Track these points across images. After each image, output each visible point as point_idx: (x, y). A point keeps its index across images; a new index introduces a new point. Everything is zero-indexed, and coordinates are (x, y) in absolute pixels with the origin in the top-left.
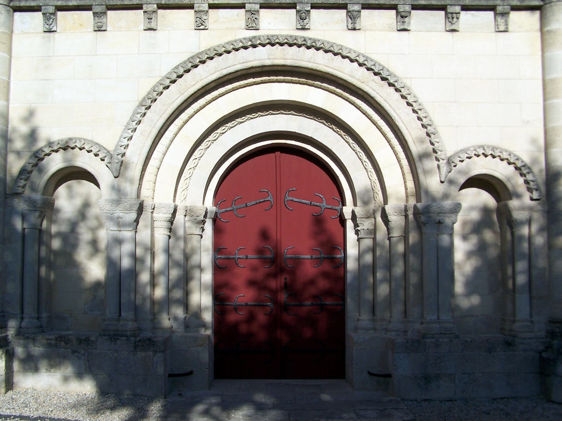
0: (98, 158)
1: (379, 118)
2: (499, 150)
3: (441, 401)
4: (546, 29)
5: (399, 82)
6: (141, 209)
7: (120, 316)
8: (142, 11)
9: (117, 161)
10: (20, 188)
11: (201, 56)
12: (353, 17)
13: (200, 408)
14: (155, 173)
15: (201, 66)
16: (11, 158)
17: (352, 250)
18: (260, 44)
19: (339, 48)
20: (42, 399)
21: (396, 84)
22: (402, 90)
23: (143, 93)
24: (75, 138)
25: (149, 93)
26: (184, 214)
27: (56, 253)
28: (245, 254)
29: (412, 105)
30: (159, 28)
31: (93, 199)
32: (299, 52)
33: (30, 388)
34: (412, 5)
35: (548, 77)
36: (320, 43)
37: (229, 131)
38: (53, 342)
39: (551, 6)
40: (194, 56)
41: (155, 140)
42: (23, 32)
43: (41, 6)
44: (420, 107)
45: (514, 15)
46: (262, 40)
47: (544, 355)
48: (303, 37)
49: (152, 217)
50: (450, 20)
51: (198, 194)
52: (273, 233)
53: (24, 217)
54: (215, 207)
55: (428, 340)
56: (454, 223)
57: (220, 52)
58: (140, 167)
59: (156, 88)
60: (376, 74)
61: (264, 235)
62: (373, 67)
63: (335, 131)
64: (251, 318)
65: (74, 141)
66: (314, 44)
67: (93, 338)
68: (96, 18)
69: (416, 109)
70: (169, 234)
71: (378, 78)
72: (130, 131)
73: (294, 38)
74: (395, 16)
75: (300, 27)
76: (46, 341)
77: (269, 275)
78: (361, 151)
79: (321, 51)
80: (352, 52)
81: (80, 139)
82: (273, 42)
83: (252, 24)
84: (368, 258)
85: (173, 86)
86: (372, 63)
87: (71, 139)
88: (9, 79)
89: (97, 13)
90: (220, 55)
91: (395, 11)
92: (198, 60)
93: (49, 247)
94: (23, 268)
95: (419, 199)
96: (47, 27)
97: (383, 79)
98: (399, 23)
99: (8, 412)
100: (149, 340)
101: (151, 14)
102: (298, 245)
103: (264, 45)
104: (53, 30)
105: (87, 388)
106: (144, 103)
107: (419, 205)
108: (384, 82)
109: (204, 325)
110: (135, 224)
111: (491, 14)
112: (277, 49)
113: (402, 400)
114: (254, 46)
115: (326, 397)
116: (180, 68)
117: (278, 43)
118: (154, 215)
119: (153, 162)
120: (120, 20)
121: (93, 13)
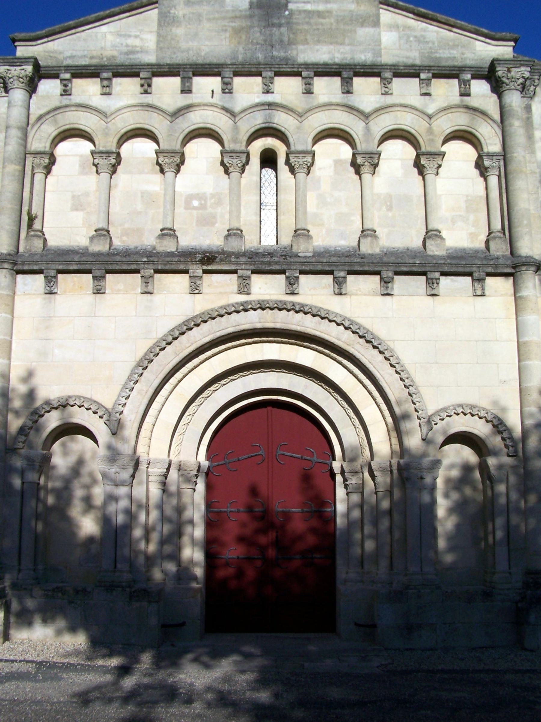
0: (97, 416)
1: (365, 378)
2: (477, 409)
3: (423, 651)
4: (518, 295)
5: (383, 345)
6: (137, 464)
7: (115, 567)
8: (139, 275)
9: (115, 419)
10: (21, 444)
11: (195, 320)
12: (339, 283)
13: (190, 656)
14: (151, 429)
15: (195, 329)
16: (10, 417)
17: (341, 507)
18: (251, 308)
19: (326, 312)
20: (39, 648)
21: (380, 346)
22: (386, 352)
23: (141, 353)
24: (75, 396)
25: (146, 354)
26: (178, 468)
27: (49, 509)
28: (234, 508)
29: (395, 367)
30: (155, 291)
31: (88, 456)
32: (288, 315)
33: (26, 639)
34: (394, 271)
35: (520, 340)
36: (308, 308)
37: (222, 388)
38: (50, 593)
39: (521, 274)
40: (189, 320)
41: (151, 398)
42: (25, 294)
43: (43, 270)
44: (402, 369)
45: (490, 281)
46: (253, 305)
47: (520, 605)
48: (292, 302)
49: (147, 472)
50: (431, 285)
51: (193, 451)
52: (263, 490)
53: (22, 473)
54: (208, 462)
55: (410, 591)
56: (435, 479)
57: (214, 316)
58: (137, 425)
59: (153, 350)
60: (361, 337)
61: (254, 492)
62: (358, 331)
63: (324, 389)
64: (240, 574)
65: (74, 399)
66: (302, 309)
67: (89, 589)
68: (96, 281)
69: (398, 370)
70: (163, 488)
71: (362, 341)
72: (127, 390)
73: (283, 303)
74: (379, 281)
75: (290, 292)
76: (43, 592)
77: (258, 531)
78: (348, 408)
79: (309, 316)
80: (338, 316)
81: (80, 397)
82: (263, 307)
83: (244, 288)
84: (356, 514)
85: (169, 348)
86: (357, 327)
87: (70, 397)
88: (11, 338)
89: (96, 277)
90: (214, 318)
91: (379, 276)
92: (193, 323)
93: (45, 503)
94: (21, 520)
95: (402, 457)
96: (48, 289)
97: (368, 342)
98: (382, 288)
99: (12, 658)
100: (145, 590)
101: (147, 278)
102: (287, 501)
103: (255, 310)
104: (53, 292)
105: (79, 641)
106: (141, 364)
107: (402, 461)
108: (368, 344)
109: (195, 578)
110: (132, 478)
111: (469, 279)
112: (268, 313)
113: (385, 649)
114: (246, 310)
115: (312, 648)
116: (176, 330)
117: (268, 307)
118: (149, 469)
119: (149, 419)
120: (119, 283)
121: (93, 277)
